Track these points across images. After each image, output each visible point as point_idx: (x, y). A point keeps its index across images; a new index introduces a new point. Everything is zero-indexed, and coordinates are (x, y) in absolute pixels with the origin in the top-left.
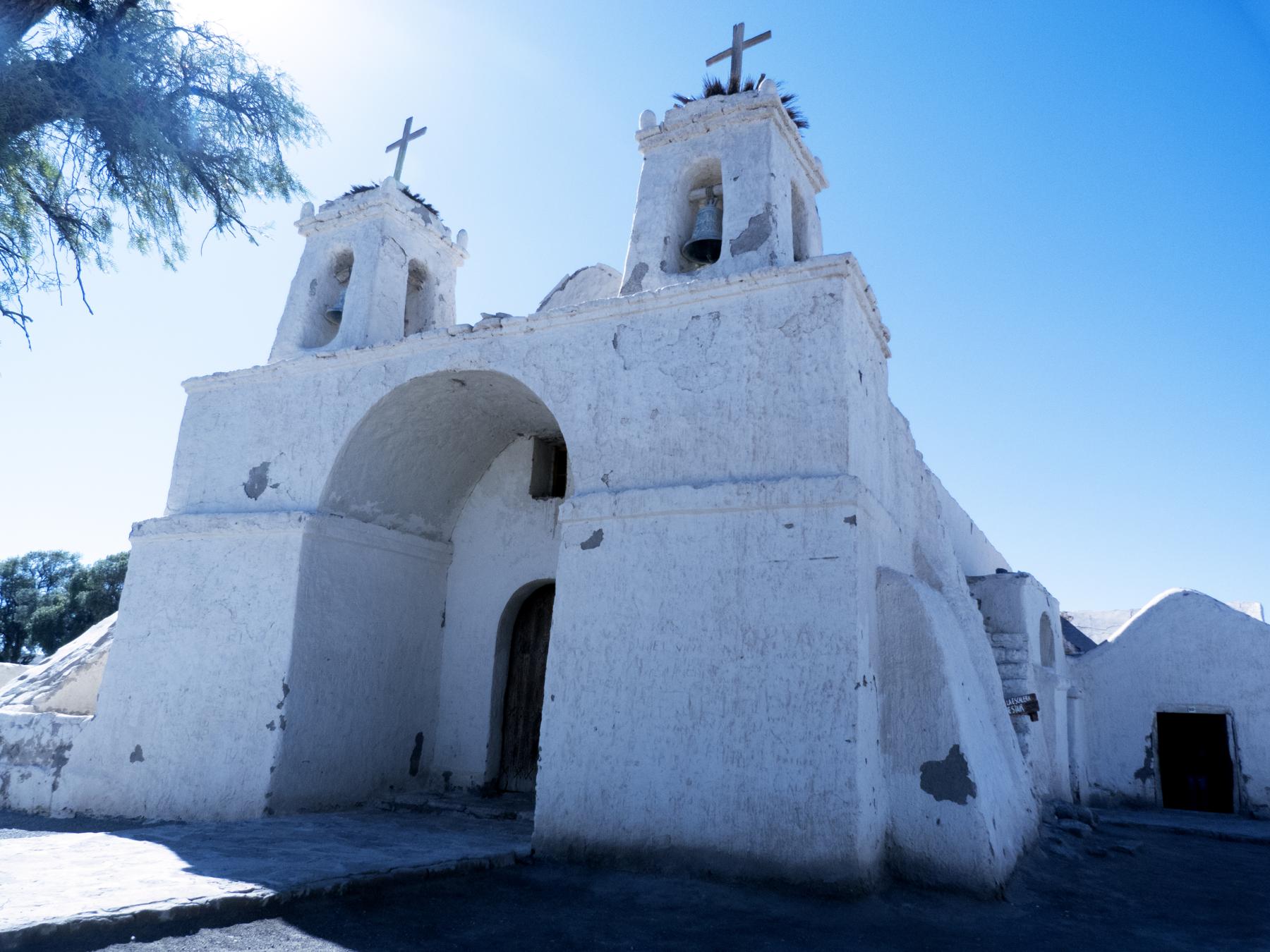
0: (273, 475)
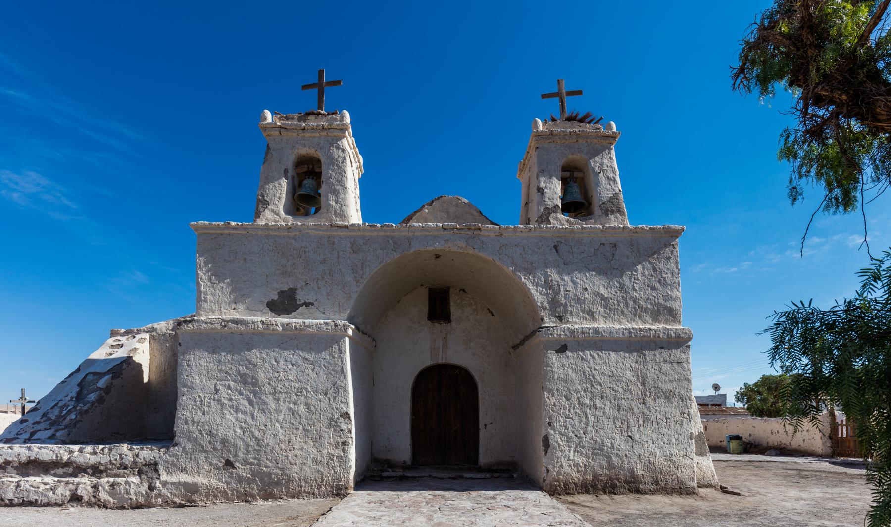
0: (301, 297)
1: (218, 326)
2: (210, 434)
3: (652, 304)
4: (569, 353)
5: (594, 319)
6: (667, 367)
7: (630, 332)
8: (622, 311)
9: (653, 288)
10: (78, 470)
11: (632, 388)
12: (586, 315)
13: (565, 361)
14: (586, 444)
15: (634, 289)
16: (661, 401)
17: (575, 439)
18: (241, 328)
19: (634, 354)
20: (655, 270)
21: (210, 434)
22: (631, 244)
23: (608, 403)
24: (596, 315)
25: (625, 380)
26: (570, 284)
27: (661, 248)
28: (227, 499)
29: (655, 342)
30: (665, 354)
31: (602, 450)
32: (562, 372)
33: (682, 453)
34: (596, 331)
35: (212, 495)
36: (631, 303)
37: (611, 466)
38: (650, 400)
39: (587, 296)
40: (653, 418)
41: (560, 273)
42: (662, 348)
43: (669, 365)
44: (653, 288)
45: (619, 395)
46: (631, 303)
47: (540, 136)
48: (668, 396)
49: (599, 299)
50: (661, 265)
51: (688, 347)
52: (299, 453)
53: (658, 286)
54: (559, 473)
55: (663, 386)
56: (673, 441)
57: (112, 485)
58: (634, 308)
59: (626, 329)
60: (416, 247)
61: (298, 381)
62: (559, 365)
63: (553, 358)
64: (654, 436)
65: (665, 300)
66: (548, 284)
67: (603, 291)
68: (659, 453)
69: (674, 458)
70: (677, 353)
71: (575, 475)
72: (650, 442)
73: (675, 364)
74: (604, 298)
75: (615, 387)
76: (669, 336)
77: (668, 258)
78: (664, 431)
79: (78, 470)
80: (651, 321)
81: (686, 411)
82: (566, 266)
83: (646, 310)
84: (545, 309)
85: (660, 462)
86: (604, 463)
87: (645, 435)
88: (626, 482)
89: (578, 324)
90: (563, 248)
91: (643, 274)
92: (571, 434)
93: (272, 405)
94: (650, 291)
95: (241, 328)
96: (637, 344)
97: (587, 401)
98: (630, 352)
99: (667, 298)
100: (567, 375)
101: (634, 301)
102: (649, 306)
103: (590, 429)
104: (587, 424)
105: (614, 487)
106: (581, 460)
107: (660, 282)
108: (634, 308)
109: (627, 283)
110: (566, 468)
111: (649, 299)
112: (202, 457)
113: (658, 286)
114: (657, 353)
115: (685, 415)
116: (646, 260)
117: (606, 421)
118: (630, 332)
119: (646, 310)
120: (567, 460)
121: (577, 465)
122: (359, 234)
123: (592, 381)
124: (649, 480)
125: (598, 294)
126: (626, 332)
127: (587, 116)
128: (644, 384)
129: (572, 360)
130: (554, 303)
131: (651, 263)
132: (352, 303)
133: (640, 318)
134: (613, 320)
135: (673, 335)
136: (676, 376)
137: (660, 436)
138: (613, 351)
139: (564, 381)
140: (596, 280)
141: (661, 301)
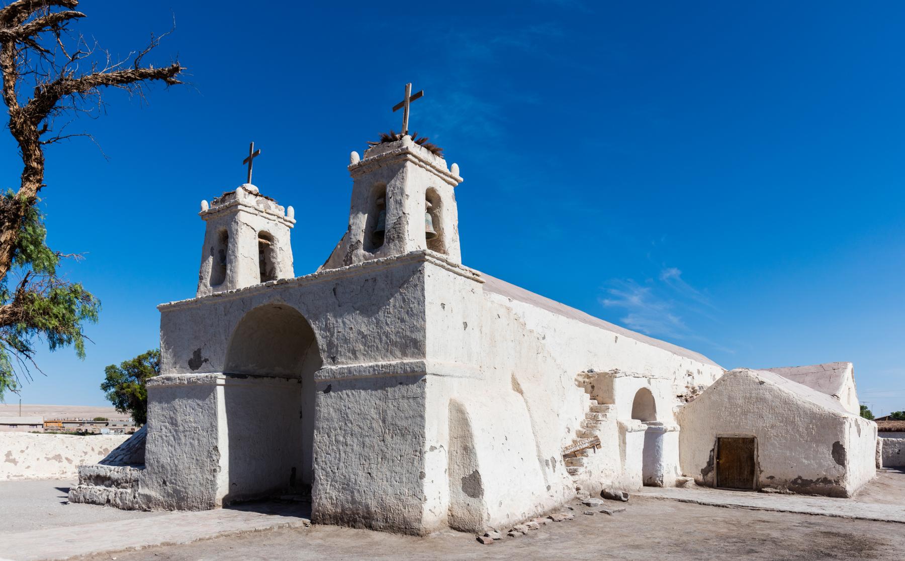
1: (160, 383)
2: (158, 462)
3: (400, 337)
4: (332, 393)
5: (356, 358)
6: (404, 404)
7: (374, 370)
8: (377, 347)
9: (403, 321)
10: (117, 483)
11: (375, 425)
12: (351, 355)
13: (329, 401)
14: (338, 479)
15: (387, 324)
16: (398, 439)
17: (331, 474)
18: (170, 383)
19: (379, 391)
20: (404, 300)
21: (158, 462)
22: (387, 277)
23: (356, 440)
24: (358, 354)
25: (369, 418)
26: (342, 325)
27: (409, 277)
28: (164, 508)
29: (396, 378)
30: (403, 389)
31: (348, 485)
32: (326, 411)
33: (411, 493)
34: (349, 369)
35: (158, 504)
36: (384, 338)
37: (354, 502)
38: (388, 438)
39: (352, 336)
40: (388, 456)
41: (335, 317)
42: (401, 384)
43: (406, 401)
44: (403, 321)
45: (364, 433)
46: (384, 338)
47: (205, 215)
48: (403, 433)
49: (360, 337)
50: (409, 295)
51: (425, 381)
52: (193, 476)
53: (406, 317)
54: (319, 504)
55: (399, 423)
56: (404, 479)
57: (122, 493)
58: (387, 343)
59: (371, 367)
60: (255, 305)
61: (195, 422)
62: (326, 405)
63: (322, 398)
64: (388, 474)
65: (412, 332)
66: (327, 328)
67: (364, 329)
68: (390, 490)
69: (403, 497)
70: (414, 388)
71: (329, 507)
72: (385, 479)
73: (411, 400)
74: (364, 337)
75: (362, 425)
76: (405, 371)
77: (416, 286)
78: (398, 469)
79: (117, 483)
80: (400, 356)
81: (418, 449)
82: (340, 309)
83: (395, 344)
84: (324, 351)
85: (391, 501)
86: (350, 498)
87: (382, 472)
88: (364, 517)
89: (346, 364)
90: (340, 290)
91: (394, 306)
92: (329, 469)
93: (183, 440)
94: (399, 324)
95: (170, 383)
96: (381, 381)
97: (341, 439)
98: (376, 390)
99: (414, 329)
100: (329, 414)
101: (387, 337)
102: (398, 340)
103: (342, 464)
104: (339, 460)
105: (355, 521)
106: (334, 494)
107: (408, 313)
108: (387, 343)
109: (382, 319)
110: (324, 501)
111: (398, 332)
112: (154, 476)
113: (406, 317)
114: (396, 389)
115: (418, 454)
116: (396, 292)
117: (354, 457)
118: (374, 370)
119: (395, 344)
120: (326, 495)
121: (331, 498)
122: (227, 299)
123: (345, 419)
124: (380, 517)
125: (360, 333)
126: (371, 370)
127: (424, 140)
128: (384, 421)
129: (334, 400)
130: (330, 345)
131: (401, 294)
132: (224, 359)
133: (391, 353)
134: (371, 357)
135: (409, 369)
136: (411, 413)
137: (393, 474)
138: (364, 389)
139: (327, 420)
140: (360, 318)
141: (408, 333)
